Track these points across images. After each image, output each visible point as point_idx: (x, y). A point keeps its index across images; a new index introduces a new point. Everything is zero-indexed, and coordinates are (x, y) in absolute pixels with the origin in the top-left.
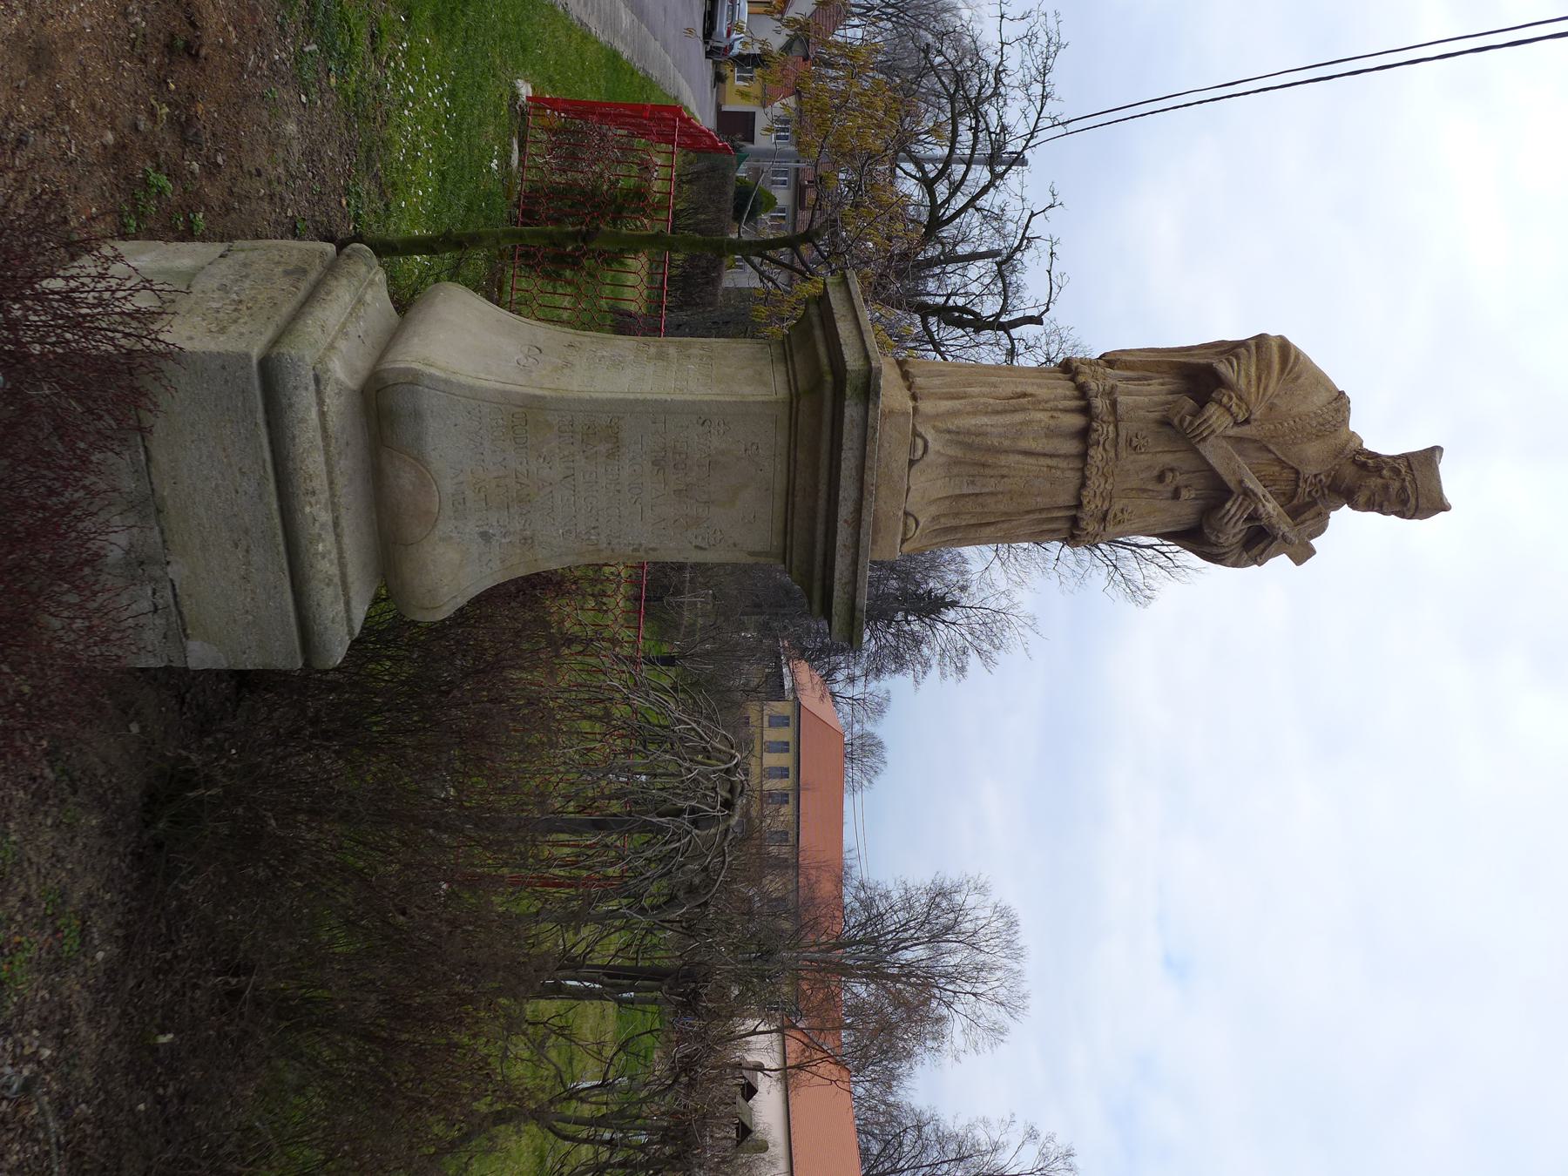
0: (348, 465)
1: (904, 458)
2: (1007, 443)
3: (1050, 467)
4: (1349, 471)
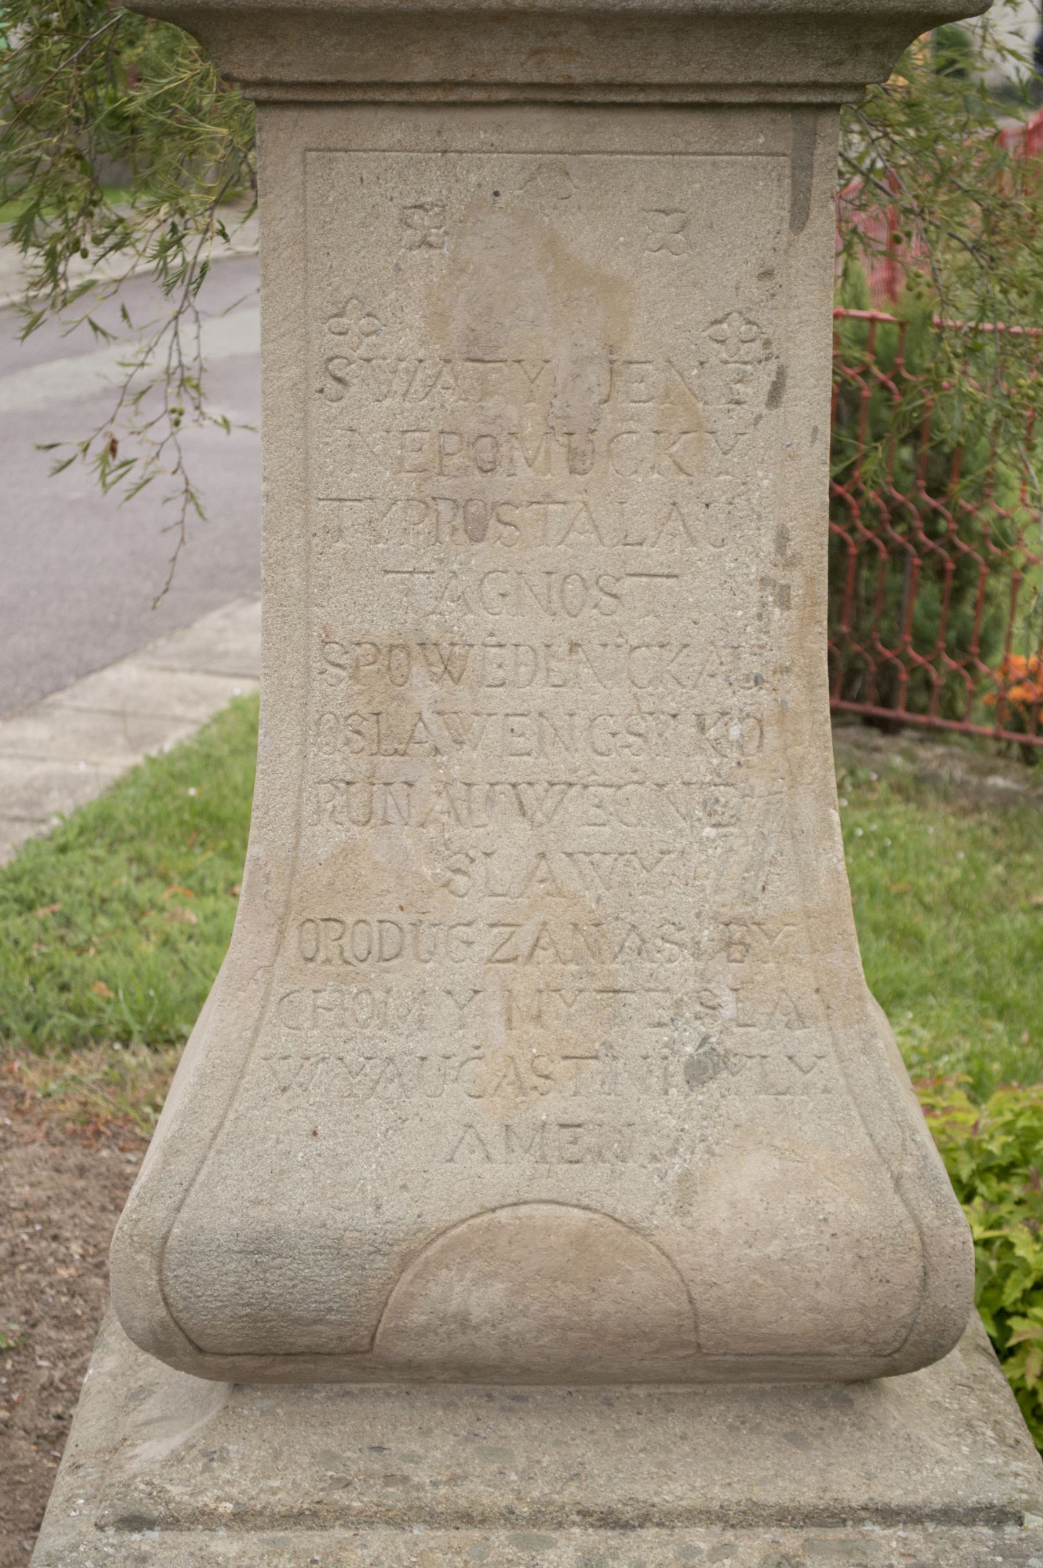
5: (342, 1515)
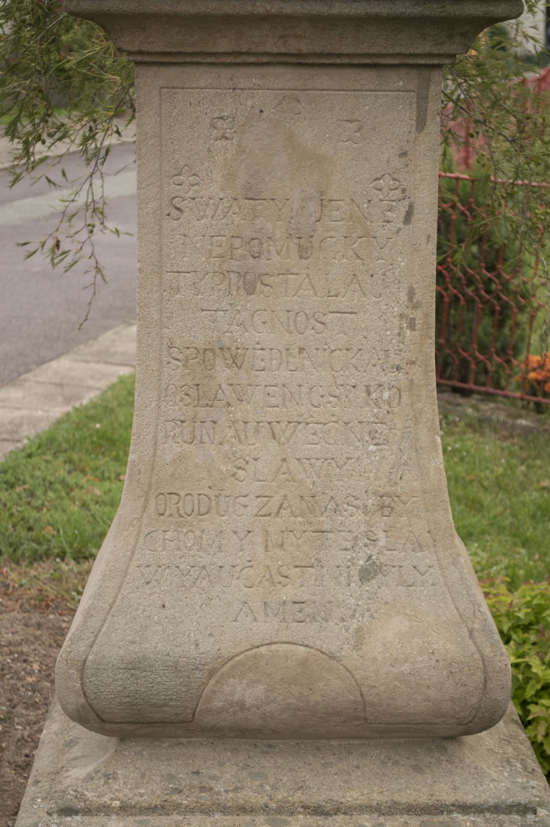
5: (177, 808)
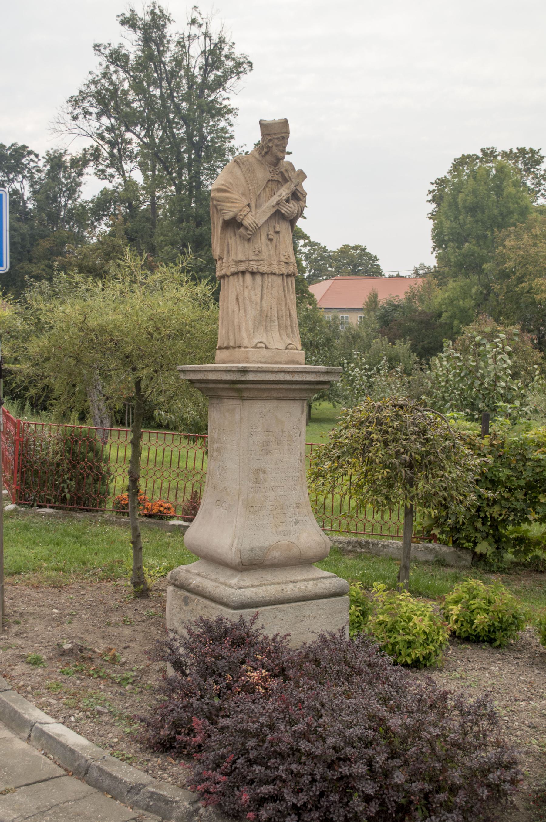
0: (269, 576)
1: (265, 351)
2: (258, 308)
3: (267, 288)
4: (269, 158)
5: (264, 584)
